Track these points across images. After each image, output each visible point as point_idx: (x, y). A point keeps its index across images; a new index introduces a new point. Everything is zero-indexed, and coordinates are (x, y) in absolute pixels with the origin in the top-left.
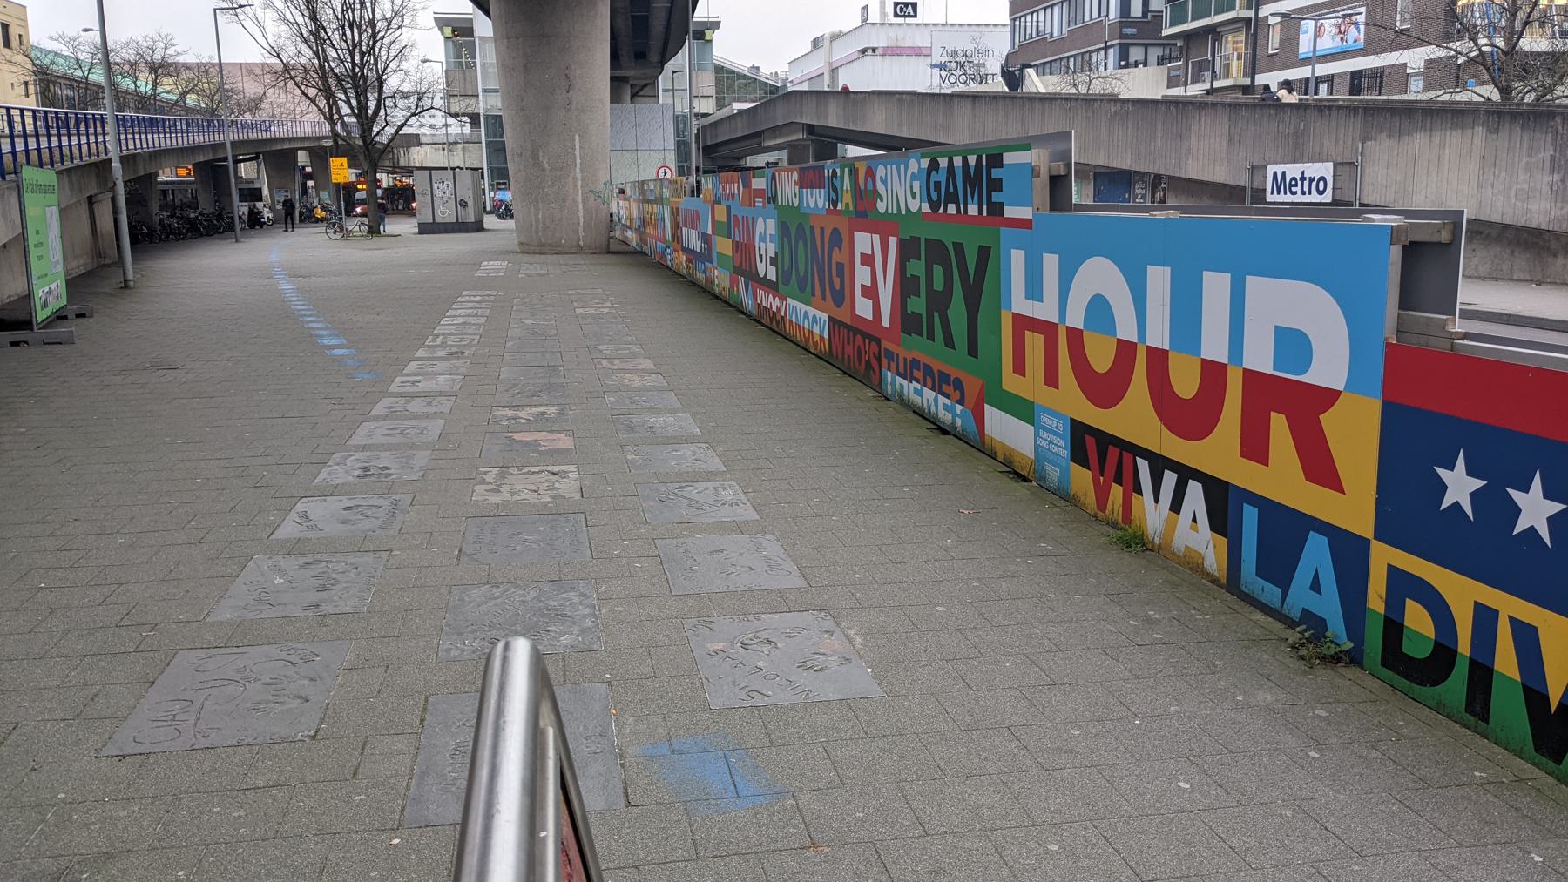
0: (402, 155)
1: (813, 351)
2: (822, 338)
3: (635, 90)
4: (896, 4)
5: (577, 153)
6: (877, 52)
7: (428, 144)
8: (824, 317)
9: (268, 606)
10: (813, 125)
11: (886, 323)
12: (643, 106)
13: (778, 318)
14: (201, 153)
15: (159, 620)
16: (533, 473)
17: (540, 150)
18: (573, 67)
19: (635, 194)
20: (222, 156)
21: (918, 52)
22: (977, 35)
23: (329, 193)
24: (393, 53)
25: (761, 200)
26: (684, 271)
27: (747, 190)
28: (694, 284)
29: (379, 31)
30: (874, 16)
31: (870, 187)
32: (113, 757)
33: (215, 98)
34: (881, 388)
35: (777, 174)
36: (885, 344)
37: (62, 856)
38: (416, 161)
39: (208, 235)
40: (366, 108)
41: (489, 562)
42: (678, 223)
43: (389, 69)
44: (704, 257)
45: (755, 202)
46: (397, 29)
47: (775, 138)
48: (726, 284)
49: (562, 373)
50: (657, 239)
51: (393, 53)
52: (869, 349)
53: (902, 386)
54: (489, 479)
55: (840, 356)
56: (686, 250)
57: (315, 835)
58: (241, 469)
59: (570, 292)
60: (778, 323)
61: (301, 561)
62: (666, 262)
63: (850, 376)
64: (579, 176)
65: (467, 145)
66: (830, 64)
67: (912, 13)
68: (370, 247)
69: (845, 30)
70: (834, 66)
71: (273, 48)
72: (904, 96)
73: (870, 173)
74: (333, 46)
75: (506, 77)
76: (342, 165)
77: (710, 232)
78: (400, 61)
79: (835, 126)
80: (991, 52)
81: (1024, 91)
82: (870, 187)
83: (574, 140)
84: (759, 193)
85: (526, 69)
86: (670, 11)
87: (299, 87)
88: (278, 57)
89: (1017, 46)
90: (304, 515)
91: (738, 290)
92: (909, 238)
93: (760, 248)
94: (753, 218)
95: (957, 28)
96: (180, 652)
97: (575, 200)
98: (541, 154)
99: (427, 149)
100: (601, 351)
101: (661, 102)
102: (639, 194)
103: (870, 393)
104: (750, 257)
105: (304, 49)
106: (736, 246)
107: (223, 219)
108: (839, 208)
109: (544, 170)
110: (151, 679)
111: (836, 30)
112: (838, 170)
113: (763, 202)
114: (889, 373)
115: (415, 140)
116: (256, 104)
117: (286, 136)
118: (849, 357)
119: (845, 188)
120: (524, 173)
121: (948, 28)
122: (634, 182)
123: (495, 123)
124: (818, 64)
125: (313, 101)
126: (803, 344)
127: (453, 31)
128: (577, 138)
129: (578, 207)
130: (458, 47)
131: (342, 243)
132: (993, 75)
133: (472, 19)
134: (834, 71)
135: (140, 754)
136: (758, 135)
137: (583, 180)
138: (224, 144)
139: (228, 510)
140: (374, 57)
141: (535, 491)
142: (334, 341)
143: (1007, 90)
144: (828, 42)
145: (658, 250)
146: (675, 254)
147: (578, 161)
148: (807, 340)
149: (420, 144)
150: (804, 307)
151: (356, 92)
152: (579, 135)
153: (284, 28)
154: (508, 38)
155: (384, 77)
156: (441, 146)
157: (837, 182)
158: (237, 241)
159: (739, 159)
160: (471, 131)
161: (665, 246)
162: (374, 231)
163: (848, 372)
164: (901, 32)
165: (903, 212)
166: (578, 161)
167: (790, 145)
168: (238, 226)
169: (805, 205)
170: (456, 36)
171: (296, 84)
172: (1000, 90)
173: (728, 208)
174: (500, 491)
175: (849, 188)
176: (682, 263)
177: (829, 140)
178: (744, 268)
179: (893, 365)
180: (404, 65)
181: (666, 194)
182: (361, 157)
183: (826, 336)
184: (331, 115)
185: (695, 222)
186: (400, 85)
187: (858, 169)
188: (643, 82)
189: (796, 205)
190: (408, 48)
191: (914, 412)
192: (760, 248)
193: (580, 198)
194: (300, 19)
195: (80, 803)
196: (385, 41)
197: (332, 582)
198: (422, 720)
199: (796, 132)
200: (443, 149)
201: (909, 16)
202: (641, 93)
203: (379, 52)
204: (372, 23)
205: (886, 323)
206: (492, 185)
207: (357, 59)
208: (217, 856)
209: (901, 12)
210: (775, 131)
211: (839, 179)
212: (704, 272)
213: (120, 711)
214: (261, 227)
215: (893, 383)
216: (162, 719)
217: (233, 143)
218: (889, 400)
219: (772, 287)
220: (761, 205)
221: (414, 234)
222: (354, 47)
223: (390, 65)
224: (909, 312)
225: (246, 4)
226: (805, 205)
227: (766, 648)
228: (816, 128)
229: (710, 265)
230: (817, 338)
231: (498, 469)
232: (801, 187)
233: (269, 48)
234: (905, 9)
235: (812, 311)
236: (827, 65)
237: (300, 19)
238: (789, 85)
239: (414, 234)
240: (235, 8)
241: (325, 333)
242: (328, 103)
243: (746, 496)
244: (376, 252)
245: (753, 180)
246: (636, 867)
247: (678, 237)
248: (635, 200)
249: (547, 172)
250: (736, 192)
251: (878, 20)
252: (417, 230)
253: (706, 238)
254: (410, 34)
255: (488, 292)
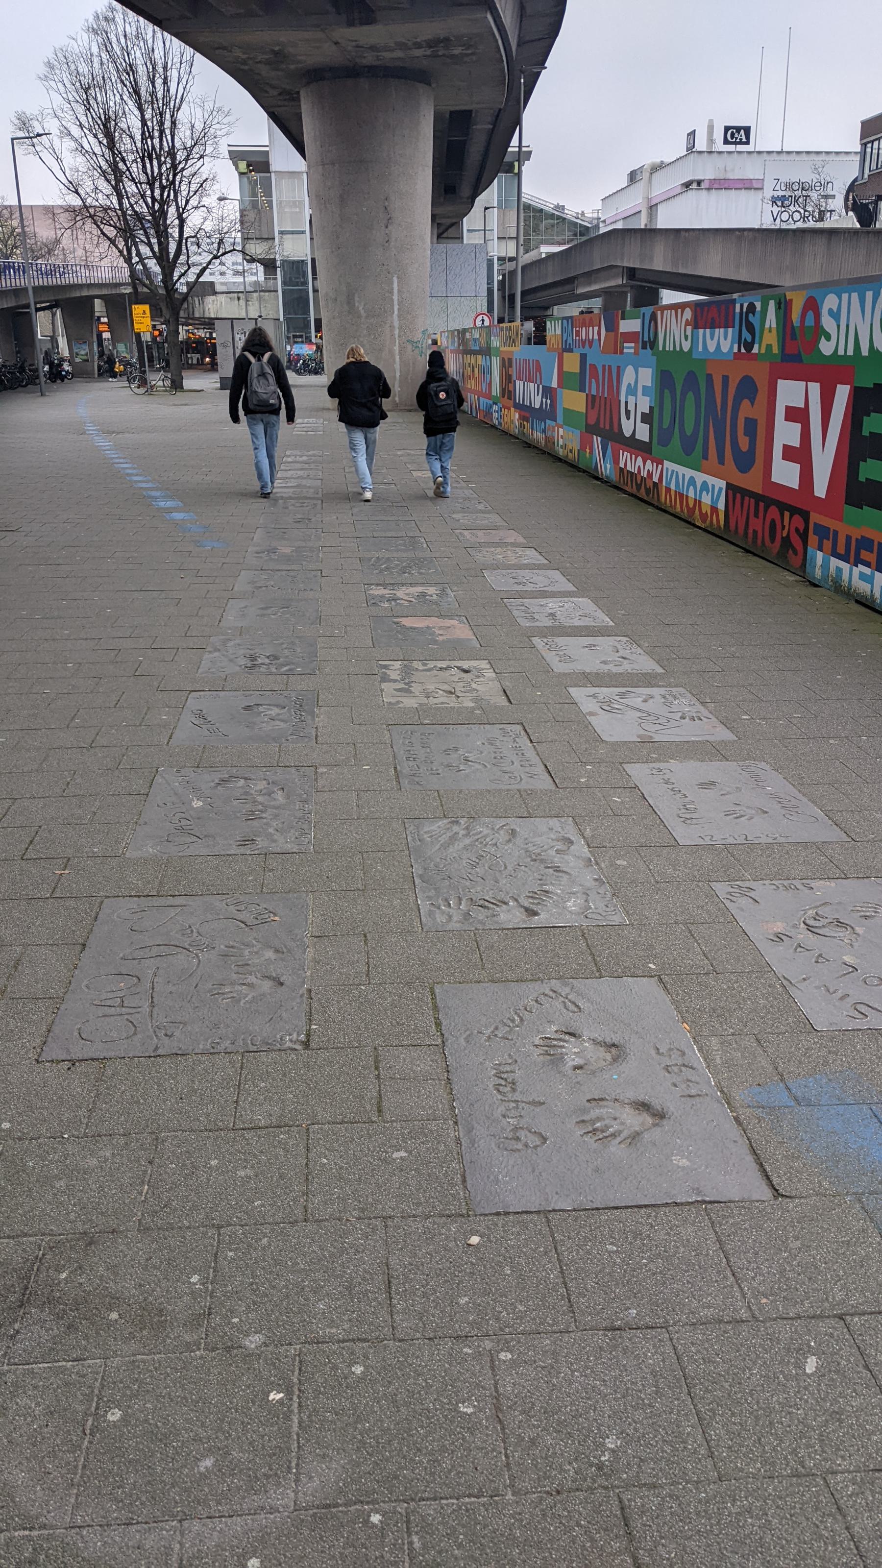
0: (197, 305)
1: (698, 524)
2: (714, 509)
3: (441, 231)
4: (727, 129)
5: (395, 297)
6: (703, 186)
7: (223, 293)
8: (722, 484)
9: (194, 839)
10: (634, 269)
11: (820, 490)
12: (451, 246)
13: (649, 484)
14: (4, 299)
15: (70, 852)
16: (441, 669)
17: (356, 295)
18: (393, 198)
19: (453, 344)
20: (24, 302)
21: (748, 185)
22: (819, 164)
23: (125, 345)
24: (194, 187)
25: (633, 345)
26: (517, 431)
27: (612, 334)
28: (529, 446)
29: (180, 163)
30: (701, 144)
31: (810, 321)
32: (58, 1062)
33: (9, 242)
34: (804, 571)
35: (659, 313)
36: (815, 518)
37: (26, 1235)
38: (211, 310)
39: (12, 388)
40: (168, 253)
41: (436, 787)
42: (510, 376)
43: (189, 207)
44: (547, 414)
45: (622, 348)
46: (199, 159)
47: (590, 284)
48: (576, 445)
49: (425, 546)
50: (480, 394)
51: (194, 187)
52: (789, 524)
53: (839, 570)
54: (394, 675)
55: (741, 530)
56: (519, 407)
57: (359, 1218)
58: (113, 654)
59: (399, 453)
60: (648, 491)
61: (216, 778)
62: (492, 420)
63: (755, 555)
64: (396, 324)
65: (262, 294)
66: (649, 200)
67: (744, 140)
68: (176, 403)
69: (667, 160)
70: (653, 203)
71: (71, 183)
72: (745, 233)
73: (812, 306)
74: (133, 180)
75: (321, 211)
76: (144, 313)
77: (554, 384)
78: (201, 197)
79: (661, 269)
80: (830, 185)
81: (877, 226)
82: (810, 321)
83: (392, 284)
84: (630, 337)
85: (343, 200)
86: (491, 133)
87: (98, 227)
88: (77, 192)
89: (866, 176)
90: (201, 715)
91: (591, 452)
92: (872, 386)
93: (626, 403)
94: (619, 367)
95: (793, 157)
96: (106, 900)
97: (391, 352)
98: (357, 299)
99: (222, 298)
100: (458, 520)
101: (465, 242)
102: (459, 345)
103: (792, 578)
104: (611, 418)
105: (102, 184)
106: (592, 401)
107: (24, 370)
108: (755, 350)
109: (359, 317)
110: (81, 941)
111: (658, 160)
112: (758, 305)
113: (635, 348)
114: (820, 554)
115: (210, 289)
116: (50, 249)
117: (84, 282)
118: (755, 532)
119: (767, 326)
120: (338, 321)
121: (784, 157)
122: (453, 332)
123: (295, 269)
124: (634, 201)
125: (113, 242)
126: (685, 515)
127: (248, 166)
128: (395, 279)
129: (394, 360)
130: (253, 184)
131: (145, 398)
132: (831, 211)
133: (268, 152)
134: (652, 208)
135: (92, 1059)
136: (571, 281)
137: (400, 328)
138: (25, 290)
139: (112, 705)
140: (174, 190)
141: (451, 693)
142: (170, 504)
143: (858, 226)
144: (648, 174)
145: (481, 407)
146: (505, 412)
147: (396, 307)
148: (691, 511)
149: (215, 293)
150: (689, 473)
151: (157, 232)
152: (398, 277)
153: (80, 159)
154: (323, 165)
155: (184, 216)
156: (236, 295)
157: (754, 320)
158: (42, 395)
159: (547, 308)
160: (265, 278)
161: (491, 402)
162: (177, 385)
163: (752, 550)
164: (730, 161)
165: (865, 352)
166: (396, 307)
167: (606, 292)
168: (43, 379)
169: (700, 349)
170: (251, 171)
171: (95, 223)
172: (850, 226)
173: (583, 357)
174: (411, 692)
175: (774, 325)
176: (513, 421)
177: (649, 285)
178: (602, 426)
179: (828, 544)
180: (206, 201)
181: (495, 342)
182: (163, 306)
183: (721, 506)
184: (130, 258)
185: (533, 372)
186: (203, 223)
187: (791, 300)
188: (448, 221)
189: (686, 349)
190: (209, 182)
191: (857, 602)
192: (626, 403)
193: (396, 348)
194: (97, 150)
195: (32, 1139)
196: (186, 173)
197: (260, 807)
198: (438, 1024)
199: (614, 277)
200: (239, 298)
201: (741, 143)
202: (445, 235)
203: (179, 187)
204: (172, 154)
205: (820, 490)
206: (288, 338)
207: (157, 193)
208: (236, 1249)
209: (732, 138)
210: (590, 276)
211: (757, 315)
212: (544, 431)
213: (52, 988)
214: (63, 381)
215: (825, 566)
216: (108, 1003)
217: (35, 289)
218: (816, 586)
219: (642, 449)
220: (632, 351)
221: (216, 389)
222: (154, 179)
223: (191, 202)
224: (862, 478)
225: (43, 132)
226: (700, 349)
227: (841, 933)
228: (637, 273)
229: (553, 423)
230: (706, 509)
231: (400, 662)
232: (696, 327)
233: (67, 183)
234: (736, 135)
235: (700, 477)
236: (646, 200)
237: (97, 150)
238: (601, 225)
239: (216, 389)
240: (31, 138)
241: (158, 494)
242: (126, 244)
243: (707, 708)
244: (185, 408)
245: (622, 322)
246: (841, 1317)
247: (510, 392)
248: (452, 352)
249: (363, 320)
250: (596, 337)
251: (704, 148)
252: (218, 385)
253: (548, 392)
254: (211, 165)
255: (314, 452)
